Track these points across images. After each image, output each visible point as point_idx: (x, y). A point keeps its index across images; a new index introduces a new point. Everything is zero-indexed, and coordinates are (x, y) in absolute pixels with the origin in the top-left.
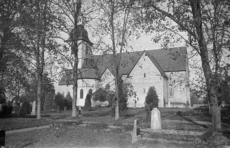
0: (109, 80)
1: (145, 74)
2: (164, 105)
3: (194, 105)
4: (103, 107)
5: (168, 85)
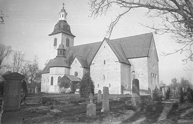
0: (77, 68)
1: (94, 64)
2: (122, 92)
3: (102, 94)
4: (66, 93)
5: (131, 72)
